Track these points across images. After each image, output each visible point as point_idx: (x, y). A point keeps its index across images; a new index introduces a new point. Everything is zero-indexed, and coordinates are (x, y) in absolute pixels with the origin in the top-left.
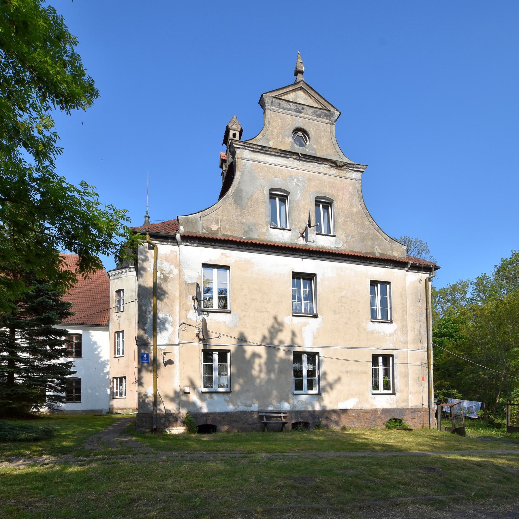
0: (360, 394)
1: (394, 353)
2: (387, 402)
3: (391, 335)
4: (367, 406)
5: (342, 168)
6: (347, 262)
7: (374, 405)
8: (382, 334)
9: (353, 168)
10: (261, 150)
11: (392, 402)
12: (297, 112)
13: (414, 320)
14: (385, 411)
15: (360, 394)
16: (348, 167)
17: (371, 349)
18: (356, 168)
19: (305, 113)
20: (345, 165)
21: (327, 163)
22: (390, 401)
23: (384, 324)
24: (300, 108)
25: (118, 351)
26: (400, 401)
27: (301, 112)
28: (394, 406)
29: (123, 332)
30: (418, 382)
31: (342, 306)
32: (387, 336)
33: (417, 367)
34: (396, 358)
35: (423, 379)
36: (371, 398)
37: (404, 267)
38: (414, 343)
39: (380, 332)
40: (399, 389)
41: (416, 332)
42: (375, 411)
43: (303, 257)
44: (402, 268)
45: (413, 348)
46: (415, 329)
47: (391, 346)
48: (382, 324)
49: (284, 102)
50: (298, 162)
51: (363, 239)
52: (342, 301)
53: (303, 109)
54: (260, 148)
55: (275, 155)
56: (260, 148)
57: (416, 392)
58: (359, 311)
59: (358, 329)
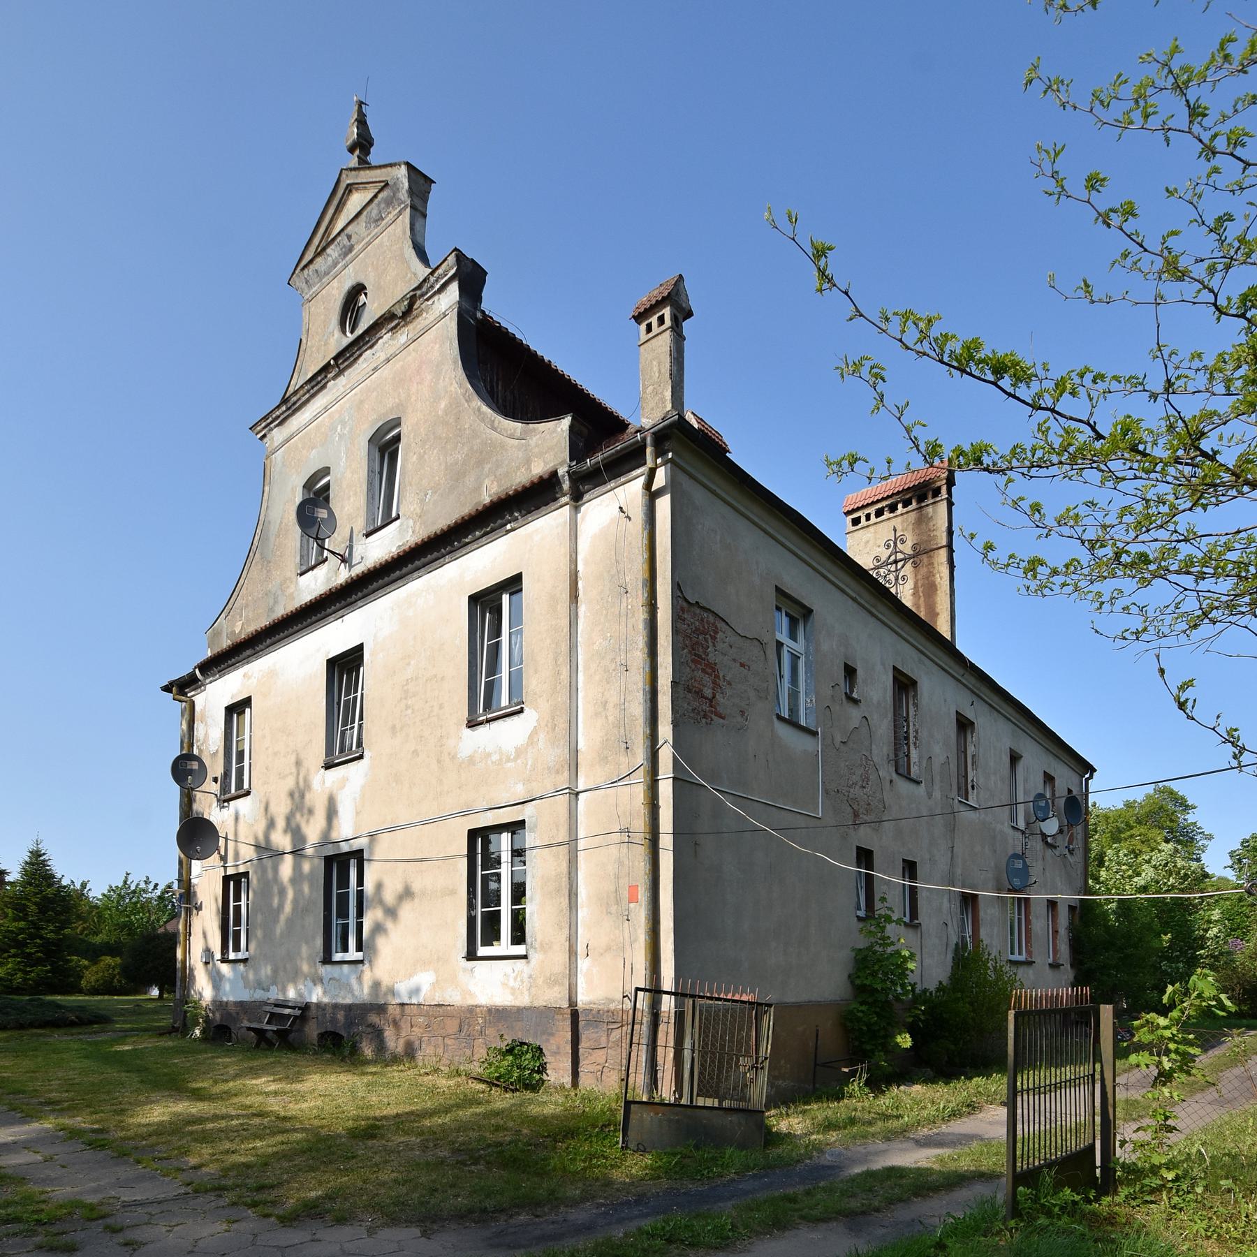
0: (438, 960)
1: (526, 813)
2: (504, 984)
3: (519, 752)
4: (454, 997)
5: (415, 313)
6: (416, 574)
7: (470, 993)
8: (495, 757)
9: (432, 287)
10: (288, 409)
11: (517, 985)
12: (346, 255)
13: (606, 670)
14: (498, 1014)
15: (438, 960)
16: (423, 295)
17: (465, 813)
18: (437, 281)
19: (358, 242)
20: (413, 300)
21: (384, 331)
22: (512, 983)
23: (500, 721)
24: (345, 241)
25: (492, 920)
26: (540, 981)
27: (351, 249)
28: (524, 1000)
29: (246, 874)
30: (614, 909)
31: (407, 707)
32: (508, 760)
33: (614, 850)
34: (532, 830)
35: (633, 898)
36: (465, 970)
37: (555, 499)
38: (604, 760)
39: (489, 755)
40: (539, 937)
41: (613, 714)
42: (472, 1010)
43: (340, 613)
44: (553, 506)
45: (600, 781)
46: (610, 706)
47: (520, 792)
48: (495, 725)
49: (319, 260)
50: (342, 380)
51: (457, 475)
52: (406, 692)
53: (349, 237)
54: (284, 408)
55: (308, 401)
56: (284, 408)
57: (608, 949)
58: (441, 707)
59: (439, 761)
